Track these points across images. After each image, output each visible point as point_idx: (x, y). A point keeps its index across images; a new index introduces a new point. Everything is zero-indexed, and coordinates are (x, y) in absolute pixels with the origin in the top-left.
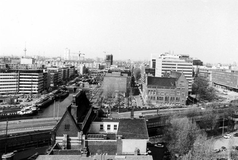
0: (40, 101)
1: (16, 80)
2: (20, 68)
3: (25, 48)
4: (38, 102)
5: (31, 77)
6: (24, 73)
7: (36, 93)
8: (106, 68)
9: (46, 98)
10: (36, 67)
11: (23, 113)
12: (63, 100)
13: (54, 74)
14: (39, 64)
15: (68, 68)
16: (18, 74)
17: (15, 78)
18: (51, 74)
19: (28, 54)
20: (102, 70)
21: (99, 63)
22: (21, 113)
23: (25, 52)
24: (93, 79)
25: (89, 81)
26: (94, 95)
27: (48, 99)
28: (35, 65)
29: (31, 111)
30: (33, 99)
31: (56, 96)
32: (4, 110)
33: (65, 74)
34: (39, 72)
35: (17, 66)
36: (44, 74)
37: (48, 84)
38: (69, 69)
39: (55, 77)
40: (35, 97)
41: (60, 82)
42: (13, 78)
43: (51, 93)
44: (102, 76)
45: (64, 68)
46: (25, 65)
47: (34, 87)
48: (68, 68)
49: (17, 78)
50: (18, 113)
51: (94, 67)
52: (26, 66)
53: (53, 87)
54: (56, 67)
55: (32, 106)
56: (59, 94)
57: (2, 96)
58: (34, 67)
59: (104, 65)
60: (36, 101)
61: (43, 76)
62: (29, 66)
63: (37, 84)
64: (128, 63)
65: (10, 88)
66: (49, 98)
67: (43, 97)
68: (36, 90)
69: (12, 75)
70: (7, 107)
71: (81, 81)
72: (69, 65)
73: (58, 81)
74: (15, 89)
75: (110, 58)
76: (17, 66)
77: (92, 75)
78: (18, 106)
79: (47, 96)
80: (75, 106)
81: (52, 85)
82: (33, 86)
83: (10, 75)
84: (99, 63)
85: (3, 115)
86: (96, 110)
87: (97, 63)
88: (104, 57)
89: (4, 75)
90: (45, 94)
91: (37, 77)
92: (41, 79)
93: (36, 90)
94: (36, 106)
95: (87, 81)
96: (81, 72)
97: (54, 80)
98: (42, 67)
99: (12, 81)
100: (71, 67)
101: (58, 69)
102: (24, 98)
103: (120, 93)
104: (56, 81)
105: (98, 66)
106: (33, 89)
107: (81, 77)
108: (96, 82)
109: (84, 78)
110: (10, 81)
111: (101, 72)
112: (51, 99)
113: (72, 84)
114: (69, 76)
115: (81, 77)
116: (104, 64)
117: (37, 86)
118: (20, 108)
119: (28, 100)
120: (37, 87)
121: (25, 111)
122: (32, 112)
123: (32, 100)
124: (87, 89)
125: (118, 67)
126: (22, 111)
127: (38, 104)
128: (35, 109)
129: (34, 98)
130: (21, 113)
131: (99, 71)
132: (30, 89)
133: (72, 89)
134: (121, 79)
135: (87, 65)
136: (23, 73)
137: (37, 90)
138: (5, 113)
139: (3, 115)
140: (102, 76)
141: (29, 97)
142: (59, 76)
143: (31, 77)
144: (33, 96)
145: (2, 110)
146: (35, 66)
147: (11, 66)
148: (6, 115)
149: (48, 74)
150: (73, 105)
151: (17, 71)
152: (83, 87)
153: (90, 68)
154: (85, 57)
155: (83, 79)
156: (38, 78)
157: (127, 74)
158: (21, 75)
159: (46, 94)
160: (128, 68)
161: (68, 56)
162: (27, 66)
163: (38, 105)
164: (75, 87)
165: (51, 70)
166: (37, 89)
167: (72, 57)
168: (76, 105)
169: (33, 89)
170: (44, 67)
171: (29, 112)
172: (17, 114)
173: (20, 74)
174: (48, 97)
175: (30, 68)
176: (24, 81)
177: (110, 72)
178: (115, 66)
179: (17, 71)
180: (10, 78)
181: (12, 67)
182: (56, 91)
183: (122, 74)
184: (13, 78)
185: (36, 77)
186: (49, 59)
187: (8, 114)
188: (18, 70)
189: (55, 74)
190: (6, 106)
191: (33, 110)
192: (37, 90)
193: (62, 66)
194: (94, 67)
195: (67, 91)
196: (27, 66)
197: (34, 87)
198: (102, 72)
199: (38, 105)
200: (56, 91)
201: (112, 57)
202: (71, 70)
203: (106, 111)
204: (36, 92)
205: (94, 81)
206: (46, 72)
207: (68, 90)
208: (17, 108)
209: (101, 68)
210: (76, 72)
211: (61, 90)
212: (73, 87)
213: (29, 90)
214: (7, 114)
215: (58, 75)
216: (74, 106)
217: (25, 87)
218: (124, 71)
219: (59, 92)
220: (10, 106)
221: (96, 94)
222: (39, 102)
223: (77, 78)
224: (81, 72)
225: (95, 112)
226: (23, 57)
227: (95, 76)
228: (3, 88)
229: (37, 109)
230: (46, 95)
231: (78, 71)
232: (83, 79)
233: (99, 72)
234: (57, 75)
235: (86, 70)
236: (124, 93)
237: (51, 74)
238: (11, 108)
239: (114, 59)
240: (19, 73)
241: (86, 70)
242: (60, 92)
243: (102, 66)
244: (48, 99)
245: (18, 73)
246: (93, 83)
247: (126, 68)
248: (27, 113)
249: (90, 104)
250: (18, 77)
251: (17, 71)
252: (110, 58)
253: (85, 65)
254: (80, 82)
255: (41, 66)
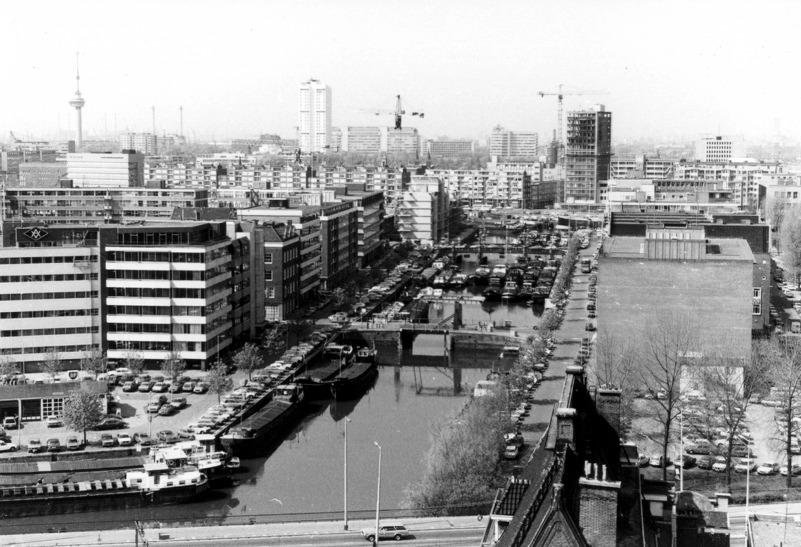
0: (231, 411)
1: (84, 286)
2: (76, 212)
3: (78, 93)
4: (220, 419)
5: (164, 266)
6: (127, 243)
7: (198, 362)
8: (570, 201)
9: (259, 393)
10: (164, 204)
11: (157, 481)
12: (348, 411)
13: (280, 245)
14: (183, 182)
15: (351, 204)
16: (97, 251)
17: (80, 277)
18: (267, 245)
19: (98, 124)
20: (546, 214)
21: (520, 169)
22: (142, 480)
23: (76, 111)
24: (503, 271)
25: (478, 284)
26: (540, 376)
27: (268, 399)
28: (156, 194)
29: (196, 475)
30: (190, 399)
31: (309, 380)
32: (54, 458)
33: (337, 243)
34: (204, 235)
35: (61, 203)
36: (231, 249)
37: (253, 305)
38: (356, 215)
39: (285, 266)
40: (198, 388)
41: (310, 291)
42: (70, 277)
43: (278, 366)
44: (555, 252)
45: (328, 209)
46: (103, 193)
47: (187, 328)
48: (351, 204)
49: (93, 276)
50: (128, 485)
51: (493, 193)
52: (110, 202)
53: (466, 367)
54: (285, 204)
55: (196, 443)
56: (328, 370)
57: (28, 376)
58: (155, 203)
59: (557, 178)
60: (210, 411)
61: (229, 258)
62: (125, 197)
63: (203, 311)
64: (709, 163)
65: (60, 331)
66: (274, 392)
67: (242, 385)
68: (198, 347)
69: (69, 259)
70: (69, 445)
71: (429, 283)
72: (356, 187)
73: (304, 291)
74: (86, 339)
75: (591, 133)
76: (61, 198)
77: (494, 241)
78: (121, 440)
79: (261, 381)
80: (605, 483)
81: (273, 314)
82: (180, 320)
83: (58, 260)
84: (520, 169)
85: (61, 489)
86: (665, 498)
87: (510, 169)
88: (553, 127)
89: (27, 260)
90: (250, 367)
91: (200, 267)
92: (218, 279)
93: (198, 347)
94: (218, 444)
95: (467, 284)
96: (422, 229)
97: (285, 283)
98: (198, 204)
99: (38, 296)
100: (366, 202)
101: (299, 213)
102: (137, 393)
103: (710, 369)
104: (292, 289)
105: (520, 185)
106: (180, 337)
107: (426, 260)
108: (524, 291)
109: (446, 268)
110: (59, 295)
111: (539, 227)
112: (284, 400)
113: (380, 304)
114: (355, 254)
115: (426, 260)
116: (557, 174)
117: (202, 320)
118: (131, 453)
119: (164, 409)
120: (204, 329)
121: (167, 472)
122: (202, 477)
123: (184, 406)
124: (482, 337)
125: (657, 191)
126: (152, 473)
127: (226, 431)
128: (216, 463)
129: (191, 391)
130: (148, 484)
131: (528, 217)
132: (165, 338)
133: (389, 339)
134: (709, 272)
135: (457, 184)
136: (120, 244)
137: (205, 347)
138: (66, 481)
139: (61, 489)
140: (555, 252)
141: (165, 389)
142: (306, 257)
143: (164, 266)
144: (188, 379)
145: (44, 459)
146: (160, 198)
147: (31, 199)
148: (72, 489)
149: (252, 247)
150: (591, 476)
151: (90, 236)
152: (456, 328)
153: (470, 202)
154: (419, 133)
155: (438, 273)
156: (203, 276)
157: (437, 190)
158: (111, 256)
159: (256, 367)
160: (724, 196)
161: (323, 129)
162: (111, 200)
163: (225, 437)
164: (409, 325)
165: (265, 225)
166: (203, 338)
167: (346, 133)
168: (610, 478)
169: (180, 337)
170: (205, 203)
171: (189, 477)
172: (124, 484)
173: (108, 249)
174: (268, 385)
175: (129, 213)
176: (132, 292)
177: (626, 225)
178: (631, 183)
179: (88, 237)
180: (59, 278)
181: (38, 208)
182: (305, 349)
183: (714, 241)
184: (70, 277)
185: (195, 264)
186: (213, 150)
187: (84, 486)
188: (97, 229)
189: (285, 249)
190: (64, 436)
191: (204, 465)
192: (205, 347)
193: (317, 195)
194: (493, 190)
195: (365, 352)
196: (116, 198)
197: (187, 328)
198: (545, 226)
199: (225, 437)
200: (305, 349)
201: (605, 121)
202: (366, 218)
203: (716, 505)
204: (199, 355)
205: (511, 286)
206: (240, 235)
207: (370, 347)
208: (120, 454)
209: (538, 196)
210: (389, 228)
211: (333, 346)
212: (398, 326)
213: (157, 346)
214: (77, 488)
215: (303, 252)
216: (595, 482)
217: (136, 328)
218: (720, 223)
219: (318, 358)
220: (80, 437)
221: (547, 374)
222: (225, 416)
223: (404, 266)
224: (422, 229)
225: (656, 510)
226: (72, 147)
227: (513, 250)
228: (28, 332)
229: (226, 459)
230: (256, 375)
231: (403, 226)
232: (438, 273)
233: (525, 227)
234: (295, 253)
235: (450, 217)
236: (740, 371)
237: (267, 245)
238: (88, 449)
239: (619, 137)
240: (102, 247)
241: (450, 217)
242: (333, 355)
243: (543, 184)
244: (268, 399)
245: (95, 244)
246: (506, 295)
247: (712, 195)
248: (176, 481)
249: (624, 460)
250: (97, 268)
251: (90, 236)
252: (591, 133)
253: (441, 186)
254: (429, 291)
255: (192, 199)
